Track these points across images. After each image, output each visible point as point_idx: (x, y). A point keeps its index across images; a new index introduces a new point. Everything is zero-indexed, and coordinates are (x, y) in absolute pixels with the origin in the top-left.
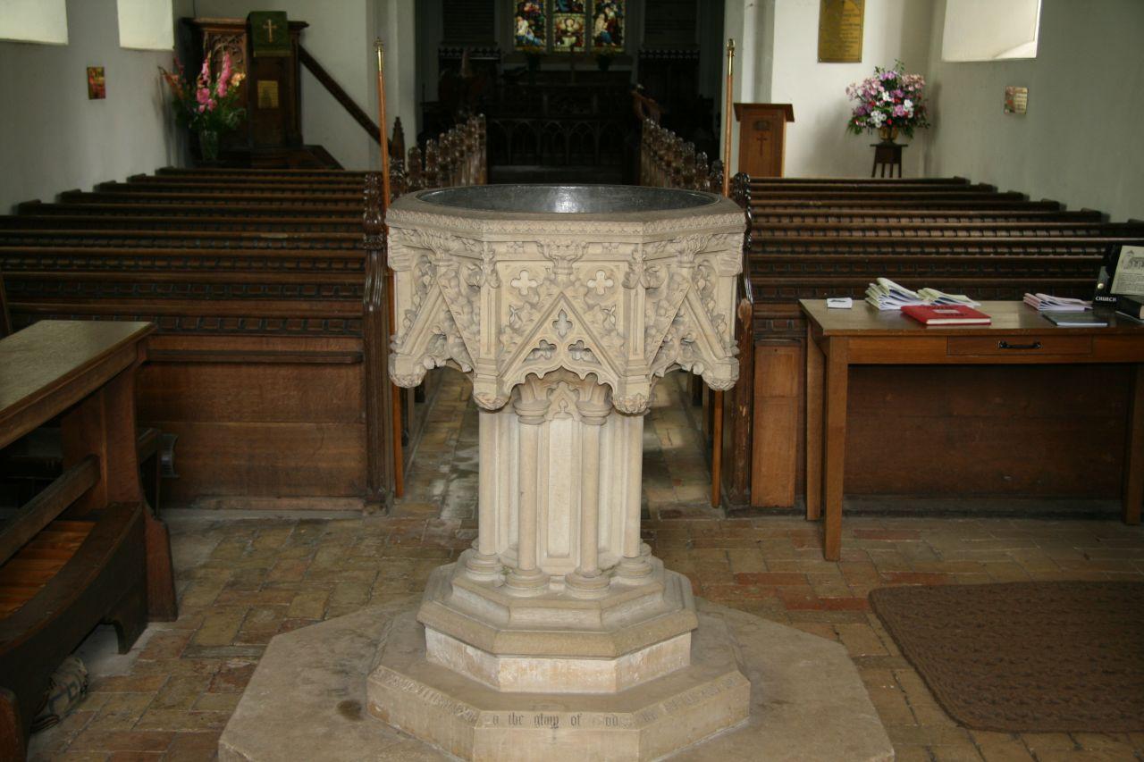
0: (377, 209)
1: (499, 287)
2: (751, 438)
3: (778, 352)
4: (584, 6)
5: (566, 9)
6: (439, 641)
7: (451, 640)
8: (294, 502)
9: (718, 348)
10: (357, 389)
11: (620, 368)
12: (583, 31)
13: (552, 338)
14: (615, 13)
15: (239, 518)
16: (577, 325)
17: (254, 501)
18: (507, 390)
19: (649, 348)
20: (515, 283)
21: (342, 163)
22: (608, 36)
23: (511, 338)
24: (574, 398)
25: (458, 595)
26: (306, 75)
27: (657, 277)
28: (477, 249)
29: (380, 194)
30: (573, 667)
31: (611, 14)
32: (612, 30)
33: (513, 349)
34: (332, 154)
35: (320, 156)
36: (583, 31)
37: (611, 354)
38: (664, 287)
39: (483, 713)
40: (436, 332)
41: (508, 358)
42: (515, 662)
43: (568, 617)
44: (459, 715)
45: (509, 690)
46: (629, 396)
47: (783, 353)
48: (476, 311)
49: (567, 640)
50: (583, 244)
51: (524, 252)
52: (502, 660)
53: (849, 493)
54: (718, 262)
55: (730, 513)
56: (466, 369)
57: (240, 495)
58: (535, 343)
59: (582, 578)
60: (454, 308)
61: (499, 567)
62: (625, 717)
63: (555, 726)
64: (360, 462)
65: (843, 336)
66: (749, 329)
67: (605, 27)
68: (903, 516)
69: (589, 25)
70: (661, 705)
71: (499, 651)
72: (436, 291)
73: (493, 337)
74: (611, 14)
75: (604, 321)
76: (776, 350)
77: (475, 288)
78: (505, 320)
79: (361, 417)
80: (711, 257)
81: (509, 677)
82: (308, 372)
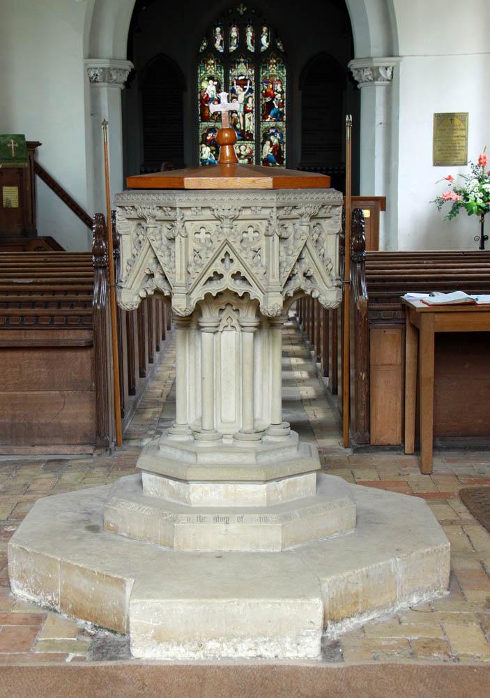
0: (102, 239)
1: (186, 237)
2: (369, 395)
3: (386, 333)
4: (254, 134)
5: (240, 138)
6: (150, 480)
7: (159, 478)
8: (44, 449)
9: (327, 279)
10: (88, 367)
11: (264, 287)
12: (253, 154)
13: (220, 270)
14: (279, 140)
15: (5, 460)
16: (236, 261)
17: (15, 449)
18: (193, 304)
19: (282, 276)
20: (197, 236)
21: (65, 248)
22: (273, 158)
23: (195, 269)
24: (237, 316)
25: (165, 451)
26: (40, 183)
27: (287, 232)
28: (172, 213)
29: (104, 228)
30: (238, 489)
31: (275, 141)
32: (276, 153)
33: (197, 276)
34: (133, 5)
35: (51, 243)
36: (253, 154)
37: (258, 278)
38: (291, 237)
39: (180, 515)
40: (148, 272)
41: (193, 282)
42: (201, 487)
43: (235, 458)
44: (165, 518)
45: (196, 506)
46: (270, 305)
47: (390, 333)
48: (173, 254)
49: (235, 475)
50: (239, 208)
51: (202, 214)
52: (192, 485)
53: (437, 435)
54: (325, 224)
55: (356, 450)
56: (166, 293)
57: (5, 445)
58: (210, 274)
59: (244, 435)
60: (158, 253)
61: (189, 432)
62: (273, 517)
63: (227, 523)
64: (91, 419)
65: (431, 312)
66: (365, 317)
67: (271, 151)
68: (480, 451)
69: (258, 149)
70: (296, 512)
71: (191, 478)
72: (148, 245)
73: (184, 268)
74: (275, 141)
75: (254, 257)
76: (385, 332)
77: (172, 240)
78: (191, 259)
79: (91, 386)
80: (321, 221)
81: (197, 497)
82: (54, 355)
